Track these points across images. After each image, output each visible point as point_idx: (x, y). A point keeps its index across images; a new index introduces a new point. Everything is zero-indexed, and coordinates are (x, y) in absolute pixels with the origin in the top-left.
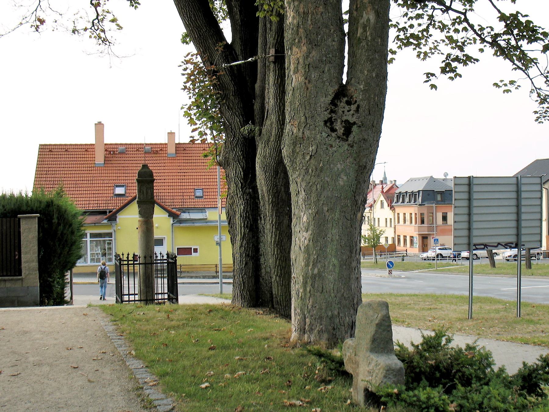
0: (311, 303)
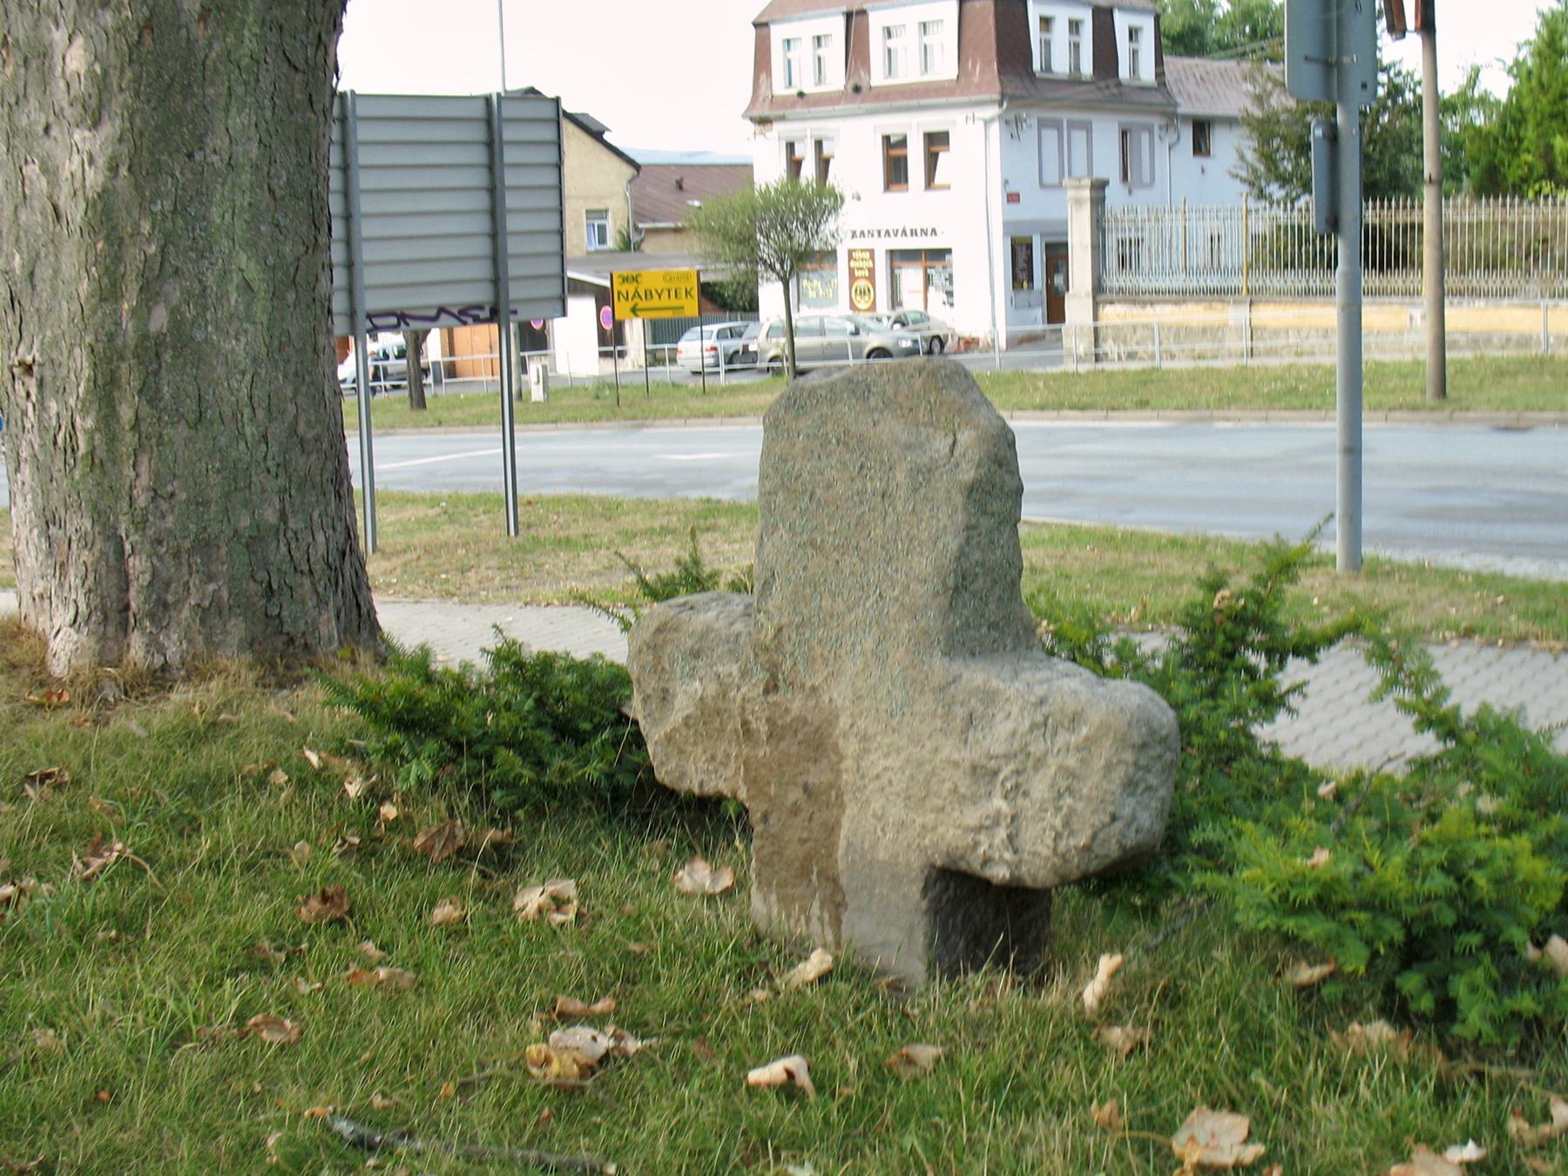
0: (144, 481)
